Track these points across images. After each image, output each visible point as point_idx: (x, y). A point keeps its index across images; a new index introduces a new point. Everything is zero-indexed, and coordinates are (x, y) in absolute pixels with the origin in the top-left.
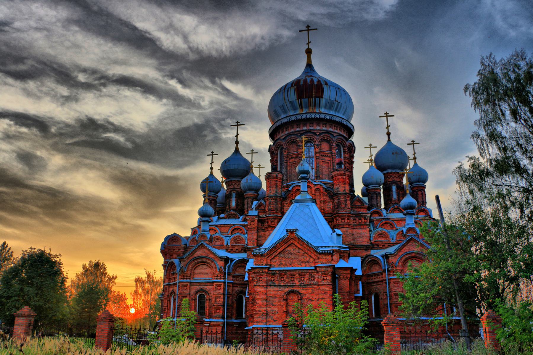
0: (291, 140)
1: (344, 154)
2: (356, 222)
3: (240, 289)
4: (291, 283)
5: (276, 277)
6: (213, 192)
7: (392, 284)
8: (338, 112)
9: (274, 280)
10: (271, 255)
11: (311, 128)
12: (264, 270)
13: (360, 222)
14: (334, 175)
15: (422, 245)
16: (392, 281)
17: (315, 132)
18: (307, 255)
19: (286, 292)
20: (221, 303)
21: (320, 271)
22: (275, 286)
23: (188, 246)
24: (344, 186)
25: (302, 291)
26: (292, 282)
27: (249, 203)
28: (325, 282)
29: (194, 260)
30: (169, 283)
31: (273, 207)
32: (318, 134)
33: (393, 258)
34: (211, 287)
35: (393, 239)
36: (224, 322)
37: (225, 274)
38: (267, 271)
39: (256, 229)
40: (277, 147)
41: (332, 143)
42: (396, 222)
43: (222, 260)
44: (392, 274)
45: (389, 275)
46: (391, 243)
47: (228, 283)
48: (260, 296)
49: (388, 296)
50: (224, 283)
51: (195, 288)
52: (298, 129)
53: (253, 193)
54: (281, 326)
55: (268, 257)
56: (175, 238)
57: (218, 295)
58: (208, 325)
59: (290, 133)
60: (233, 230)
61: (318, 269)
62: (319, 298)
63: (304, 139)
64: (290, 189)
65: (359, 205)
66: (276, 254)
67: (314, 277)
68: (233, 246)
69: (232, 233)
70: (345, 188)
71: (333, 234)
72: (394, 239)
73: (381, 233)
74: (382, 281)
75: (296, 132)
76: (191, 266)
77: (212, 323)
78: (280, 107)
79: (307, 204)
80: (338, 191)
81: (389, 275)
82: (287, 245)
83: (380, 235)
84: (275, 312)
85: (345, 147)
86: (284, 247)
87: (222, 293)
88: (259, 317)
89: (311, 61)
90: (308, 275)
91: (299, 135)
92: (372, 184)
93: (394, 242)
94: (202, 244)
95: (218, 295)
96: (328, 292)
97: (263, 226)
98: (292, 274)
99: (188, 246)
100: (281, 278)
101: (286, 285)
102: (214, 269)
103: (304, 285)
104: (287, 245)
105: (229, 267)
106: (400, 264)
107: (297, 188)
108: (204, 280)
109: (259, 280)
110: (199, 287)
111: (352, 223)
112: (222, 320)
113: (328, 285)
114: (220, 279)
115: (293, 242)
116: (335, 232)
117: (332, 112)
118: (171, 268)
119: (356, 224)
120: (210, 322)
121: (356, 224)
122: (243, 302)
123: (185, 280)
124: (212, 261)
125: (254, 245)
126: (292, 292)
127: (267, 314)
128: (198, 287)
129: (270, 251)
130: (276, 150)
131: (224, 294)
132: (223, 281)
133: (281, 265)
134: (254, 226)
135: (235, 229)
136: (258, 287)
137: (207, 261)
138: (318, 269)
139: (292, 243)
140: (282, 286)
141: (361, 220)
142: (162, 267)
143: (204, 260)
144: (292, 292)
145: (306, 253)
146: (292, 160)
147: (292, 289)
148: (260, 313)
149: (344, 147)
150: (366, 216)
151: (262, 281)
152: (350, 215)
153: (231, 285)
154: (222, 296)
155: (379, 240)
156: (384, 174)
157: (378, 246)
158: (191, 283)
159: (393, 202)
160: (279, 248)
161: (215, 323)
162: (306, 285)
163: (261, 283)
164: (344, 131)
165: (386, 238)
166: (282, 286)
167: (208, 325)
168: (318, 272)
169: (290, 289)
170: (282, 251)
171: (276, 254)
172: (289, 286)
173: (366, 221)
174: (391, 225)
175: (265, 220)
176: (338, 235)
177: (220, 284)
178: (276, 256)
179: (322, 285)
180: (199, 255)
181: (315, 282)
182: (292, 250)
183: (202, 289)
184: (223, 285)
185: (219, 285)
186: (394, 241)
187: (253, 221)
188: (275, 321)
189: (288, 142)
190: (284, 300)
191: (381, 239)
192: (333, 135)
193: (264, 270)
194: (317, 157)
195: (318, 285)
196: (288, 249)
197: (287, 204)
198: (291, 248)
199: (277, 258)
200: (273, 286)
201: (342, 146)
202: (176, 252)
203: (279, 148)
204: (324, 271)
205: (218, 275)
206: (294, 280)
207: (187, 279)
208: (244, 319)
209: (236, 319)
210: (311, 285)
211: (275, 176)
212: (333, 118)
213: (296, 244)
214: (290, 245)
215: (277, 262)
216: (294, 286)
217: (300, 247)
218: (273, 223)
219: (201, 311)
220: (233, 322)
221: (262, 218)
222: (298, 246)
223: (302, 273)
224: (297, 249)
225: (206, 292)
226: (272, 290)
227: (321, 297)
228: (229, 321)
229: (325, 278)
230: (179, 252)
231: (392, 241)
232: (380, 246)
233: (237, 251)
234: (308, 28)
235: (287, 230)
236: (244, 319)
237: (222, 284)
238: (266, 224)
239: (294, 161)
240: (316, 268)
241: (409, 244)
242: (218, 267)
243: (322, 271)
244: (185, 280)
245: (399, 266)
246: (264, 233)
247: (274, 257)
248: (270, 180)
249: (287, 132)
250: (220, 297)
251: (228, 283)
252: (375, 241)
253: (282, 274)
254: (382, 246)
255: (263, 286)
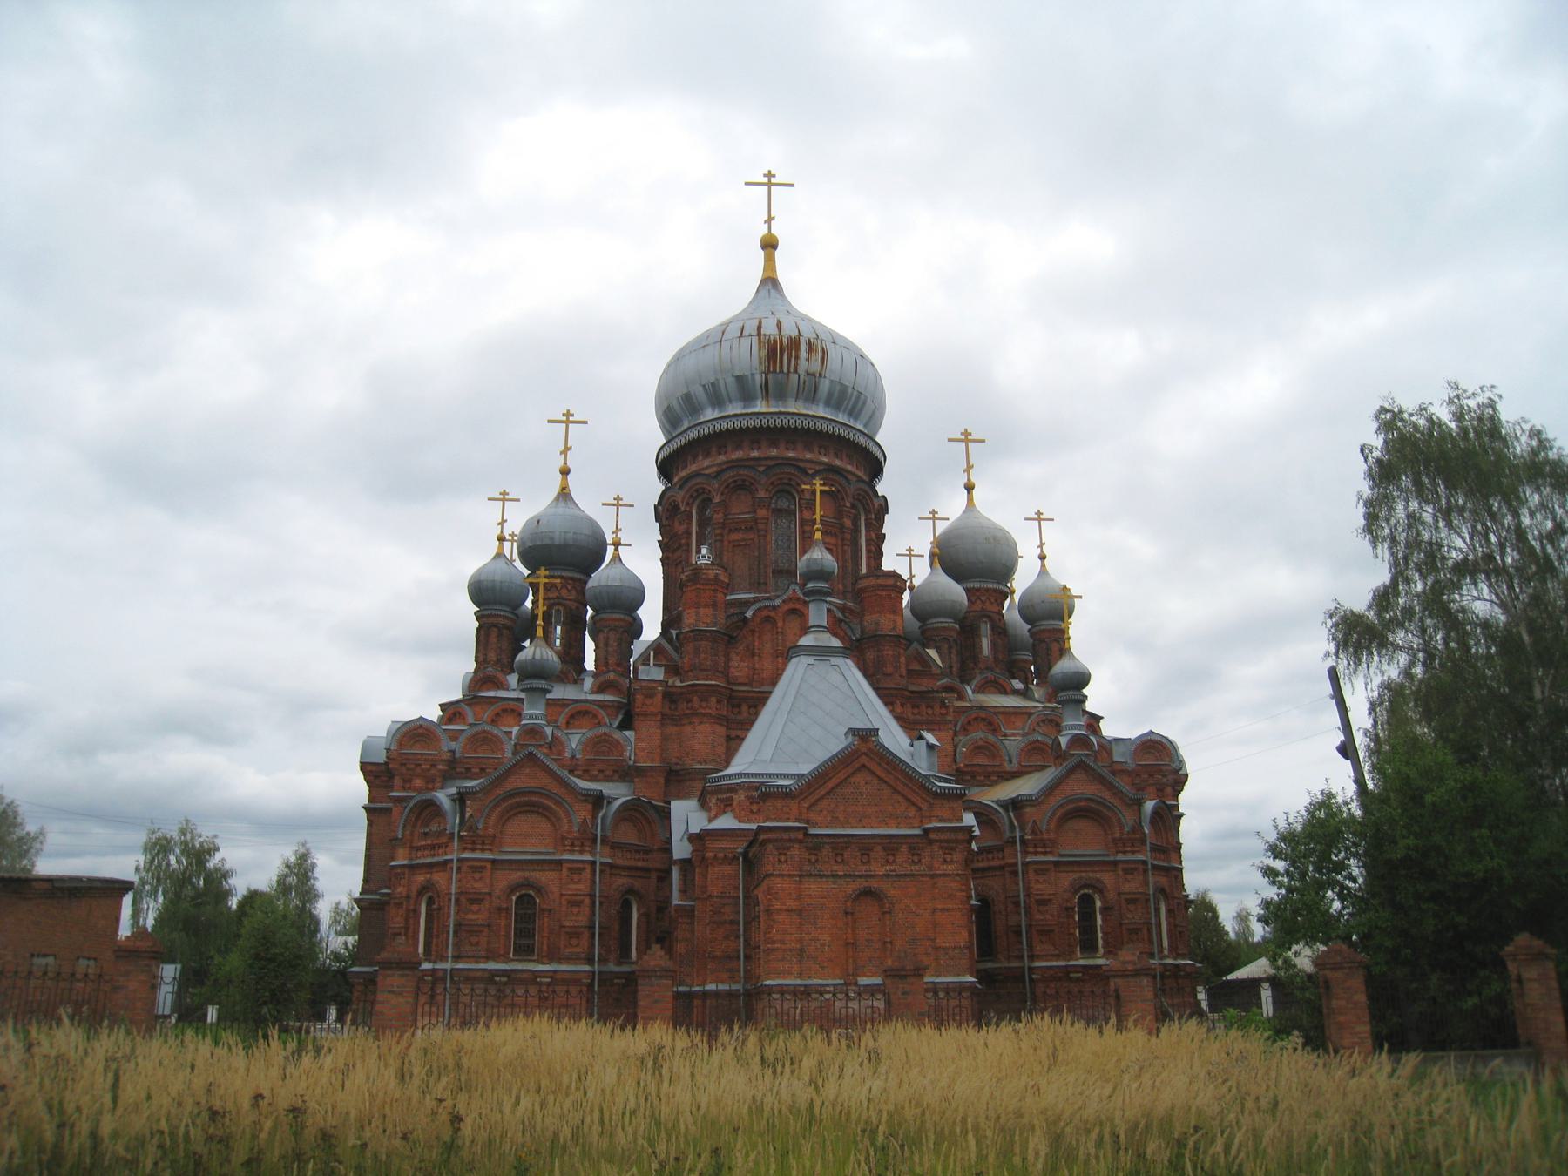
0: (735, 481)
1: (867, 531)
2: (919, 713)
3: (625, 880)
4: (863, 869)
5: (825, 852)
6: (501, 603)
7: (1032, 876)
8: (856, 419)
9: (817, 861)
10: (810, 794)
11: (791, 454)
12: (793, 835)
13: (930, 712)
14: (866, 588)
15: (1102, 780)
16: (1031, 868)
17: (801, 464)
18: (900, 799)
19: (850, 891)
20: (582, 920)
21: (937, 841)
22: (821, 876)
23: (458, 755)
24: (892, 616)
25: (891, 890)
26: (864, 868)
27: (611, 642)
28: (949, 868)
29: (504, 800)
30: (411, 859)
31: (706, 659)
32: (810, 472)
33: (1034, 809)
34: (553, 875)
35: (1011, 761)
36: (594, 973)
37: (594, 841)
38: (800, 836)
39: (659, 717)
40: (691, 496)
41: (843, 499)
42: (1000, 717)
43: (585, 801)
44: (1031, 850)
45: (1025, 853)
46: (1005, 772)
47: (601, 863)
48: (784, 904)
49: (1022, 904)
50: (593, 863)
51: (505, 879)
52: (755, 454)
53: (622, 616)
54: (842, 982)
55: (803, 800)
56: (421, 731)
57: (575, 898)
58: (548, 980)
59: (733, 461)
60: (572, 716)
61: (933, 836)
62: (935, 910)
63: (818, 488)
64: (749, 614)
65: (918, 667)
66: (823, 791)
67: (919, 855)
68: (591, 762)
69: (568, 723)
70: (895, 621)
71: (916, 743)
72: (1014, 761)
73: (981, 743)
74: (1002, 868)
75: (748, 460)
76: (493, 818)
77: (558, 976)
78: (704, 386)
79: (834, 660)
80: (876, 630)
81: (1025, 853)
82: (850, 770)
83: (978, 749)
84: (823, 945)
85: (870, 512)
86: (842, 775)
87: (587, 891)
88: (783, 959)
89: (774, 269)
90: (904, 849)
91: (761, 469)
92: (940, 616)
93: (1014, 770)
94: (531, 753)
95: (575, 898)
96: (958, 894)
97: (676, 709)
98: (865, 846)
99: (458, 755)
100: (836, 855)
101: (850, 875)
102: (566, 826)
103: (896, 875)
104: (850, 770)
105: (603, 818)
106: (1053, 825)
107: (765, 613)
108: (533, 853)
109: (780, 861)
110: (519, 873)
111: (910, 715)
112: (587, 968)
113: (958, 875)
114: (581, 852)
115: (867, 764)
116: (921, 738)
117: (841, 418)
118: (417, 819)
119: (918, 717)
120: (555, 972)
121: (918, 717)
122: (631, 918)
123: (477, 855)
124: (558, 803)
125: (653, 760)
126: (867, 893)
127: (801, 951)
128: (516, 876)
129: (809, 785)
130: (688, 504)
131: (592, 896)
132: (588, 857)
133: (835, 822)
134: (652, 709)
135: (579, 713)
136: (778, 880)
137: (542, 800)
138: (933, 836)
139: (864, 766)
140: (840, 877)
141: (932, 708)
142: (364, 813)
143: (534, 798)
144: (867, 893)
145: (899, 792)
146: (734, 536)
147: (866, 884)
148: (783, 947)
149: (867, 512)
150: (946, 698)
151: (786, 861)
152: (906, 693)
153: (489, 866)
154: (587, 901)
155: (975, 762)
156: (968, 591)
157: (973, 777)
158: (494, 861)
159: (981, 665)
160: (831, 778)
161: (567, 976)
162: (902, 875)
163: (785, 869)
164: (865, 470)
165: (994, 757)
166: (840, 877)
167: (548, 980)
168: (931, 842)
169: (860, 884)
170: (838, 785)
171: (823, 791)
172: (860, 876)
173: (944, 711)
174: (990, 723)
175: (682, 694)
176: (930, 747)
177: (580, 865)
178: (822, 798)
179: (944, 875)
180: (520, 785)
181: (922, 868)
182: (863, 782)
183: (527, 879)
184: (588, 871)
185: (579, 869)
186: (1015, 766)
187: (650, 696)
188: (823, 968)
189: (727, 487)
190: (846, 913)
191: (982, 760)
192: (846, 478)
193: (793, 835)
194: (806, 535)
195: (932, 876)
196: (852, 780)
197: (737, 654)
198: (859, 778)
199: (824, 803)
200: (816, 875)
201: (865, 509)
202: (423, 770)
203: (697, 497)
204: (947, 841)
205: (576, 843)
206: (869, 862)
207: (483, 850)
208: (633, 963)
209: (619, 964)
210: (913, 875)
211: (712, 576)
212: (847, 432)
213: (874, 767)
214: (859, 769)
215: (825, 812)
216: (871, 876)
217: (883, 775)
218: (704, 704)
219: (524, 941)
220: (611, 972)
221: (674, 690)
222: (878, 773)
223: (891, 845)
224: (876, 781)
225: (539, 890)
226: (813, 887)
227: (939, 907)
228: (605, 969)
229: (948, 857)
230: (433, 771)
231: (1008, 767)
232: (978, 778)
233: (601, 776)
234: (769, 180)
235: (853, 732)
236: (633, 963)
237: (588, 867)
238: (683, 706)
239: (744, 540)
240: (926, 831)
241: (1073, 777)
242: (577, 819)
243: (941, 841)
244: (477, 855)
245: (1048, 830)
246: (675, 728)
247: (818, 800)
248: (698, 586)
249: (722, 458)
250: (582, 902)
251: (601, 863)
252: (966, 765)
253: (841, 845)
254: (982, 778)
255: (790, 875)
